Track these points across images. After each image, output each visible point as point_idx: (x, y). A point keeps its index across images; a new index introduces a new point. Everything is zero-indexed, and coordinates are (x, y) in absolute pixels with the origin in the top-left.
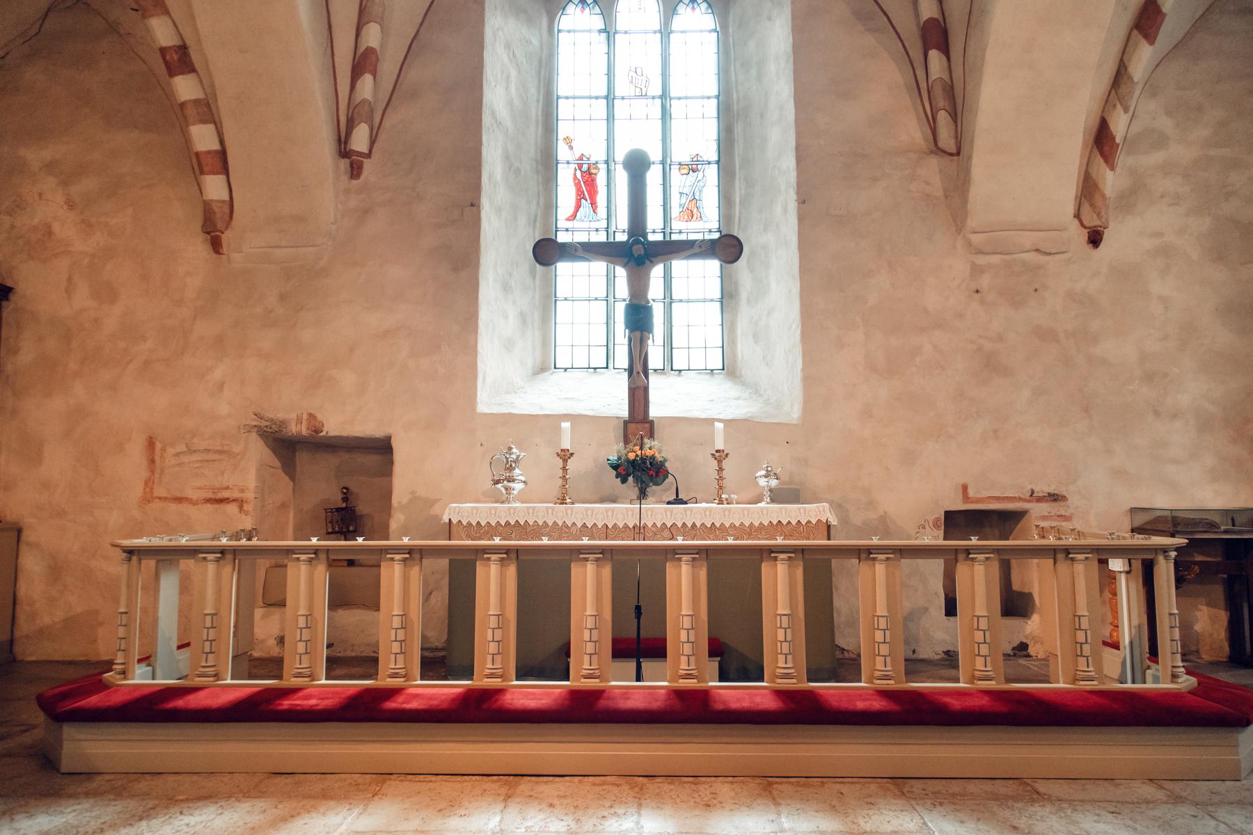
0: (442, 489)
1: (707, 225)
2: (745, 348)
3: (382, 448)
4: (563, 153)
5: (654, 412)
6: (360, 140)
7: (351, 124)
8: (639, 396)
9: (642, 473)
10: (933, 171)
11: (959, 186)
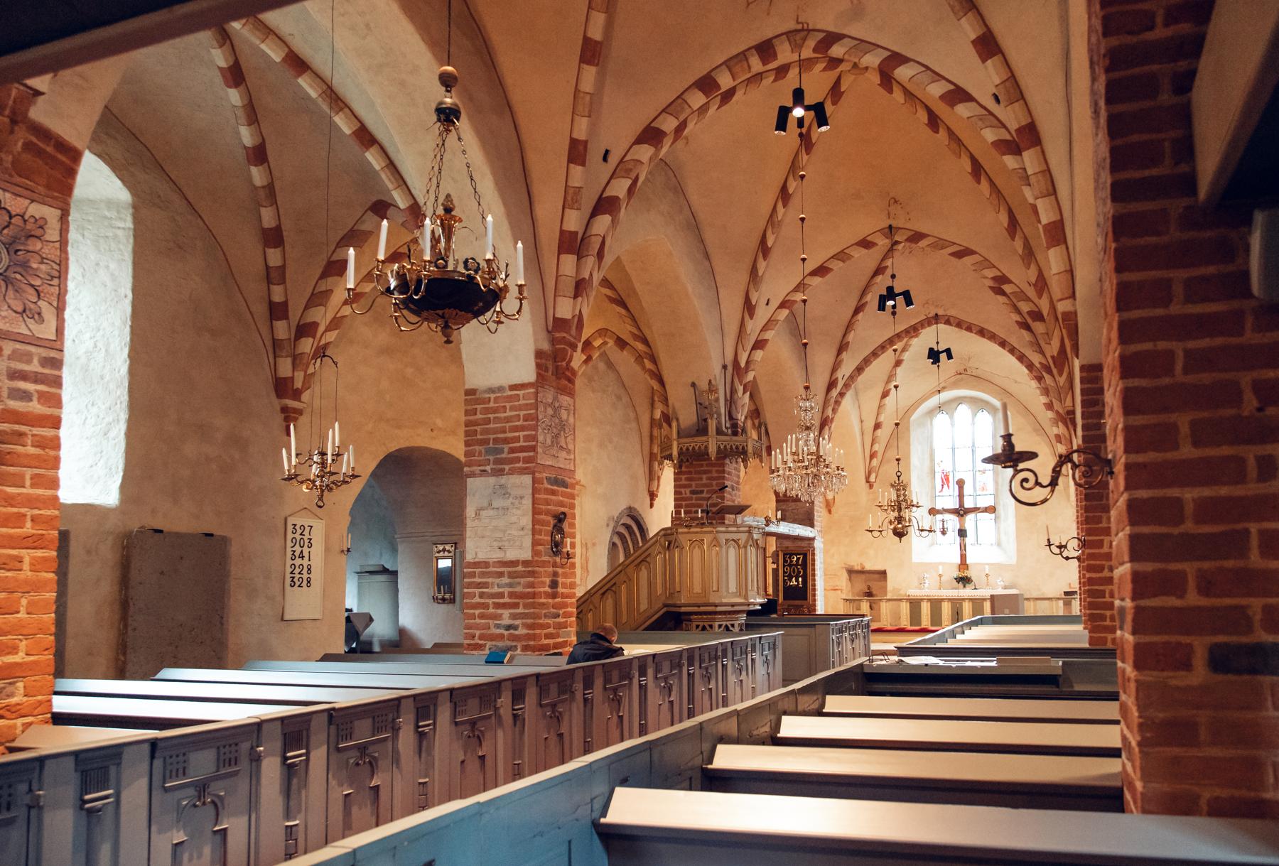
0: (901, 583)
1: (988, 502)
2: (1003, 538)
3: (884, 573)
5: (968, 562)
6: (872, 478)
8: (963, 557)
9: (964, 581)
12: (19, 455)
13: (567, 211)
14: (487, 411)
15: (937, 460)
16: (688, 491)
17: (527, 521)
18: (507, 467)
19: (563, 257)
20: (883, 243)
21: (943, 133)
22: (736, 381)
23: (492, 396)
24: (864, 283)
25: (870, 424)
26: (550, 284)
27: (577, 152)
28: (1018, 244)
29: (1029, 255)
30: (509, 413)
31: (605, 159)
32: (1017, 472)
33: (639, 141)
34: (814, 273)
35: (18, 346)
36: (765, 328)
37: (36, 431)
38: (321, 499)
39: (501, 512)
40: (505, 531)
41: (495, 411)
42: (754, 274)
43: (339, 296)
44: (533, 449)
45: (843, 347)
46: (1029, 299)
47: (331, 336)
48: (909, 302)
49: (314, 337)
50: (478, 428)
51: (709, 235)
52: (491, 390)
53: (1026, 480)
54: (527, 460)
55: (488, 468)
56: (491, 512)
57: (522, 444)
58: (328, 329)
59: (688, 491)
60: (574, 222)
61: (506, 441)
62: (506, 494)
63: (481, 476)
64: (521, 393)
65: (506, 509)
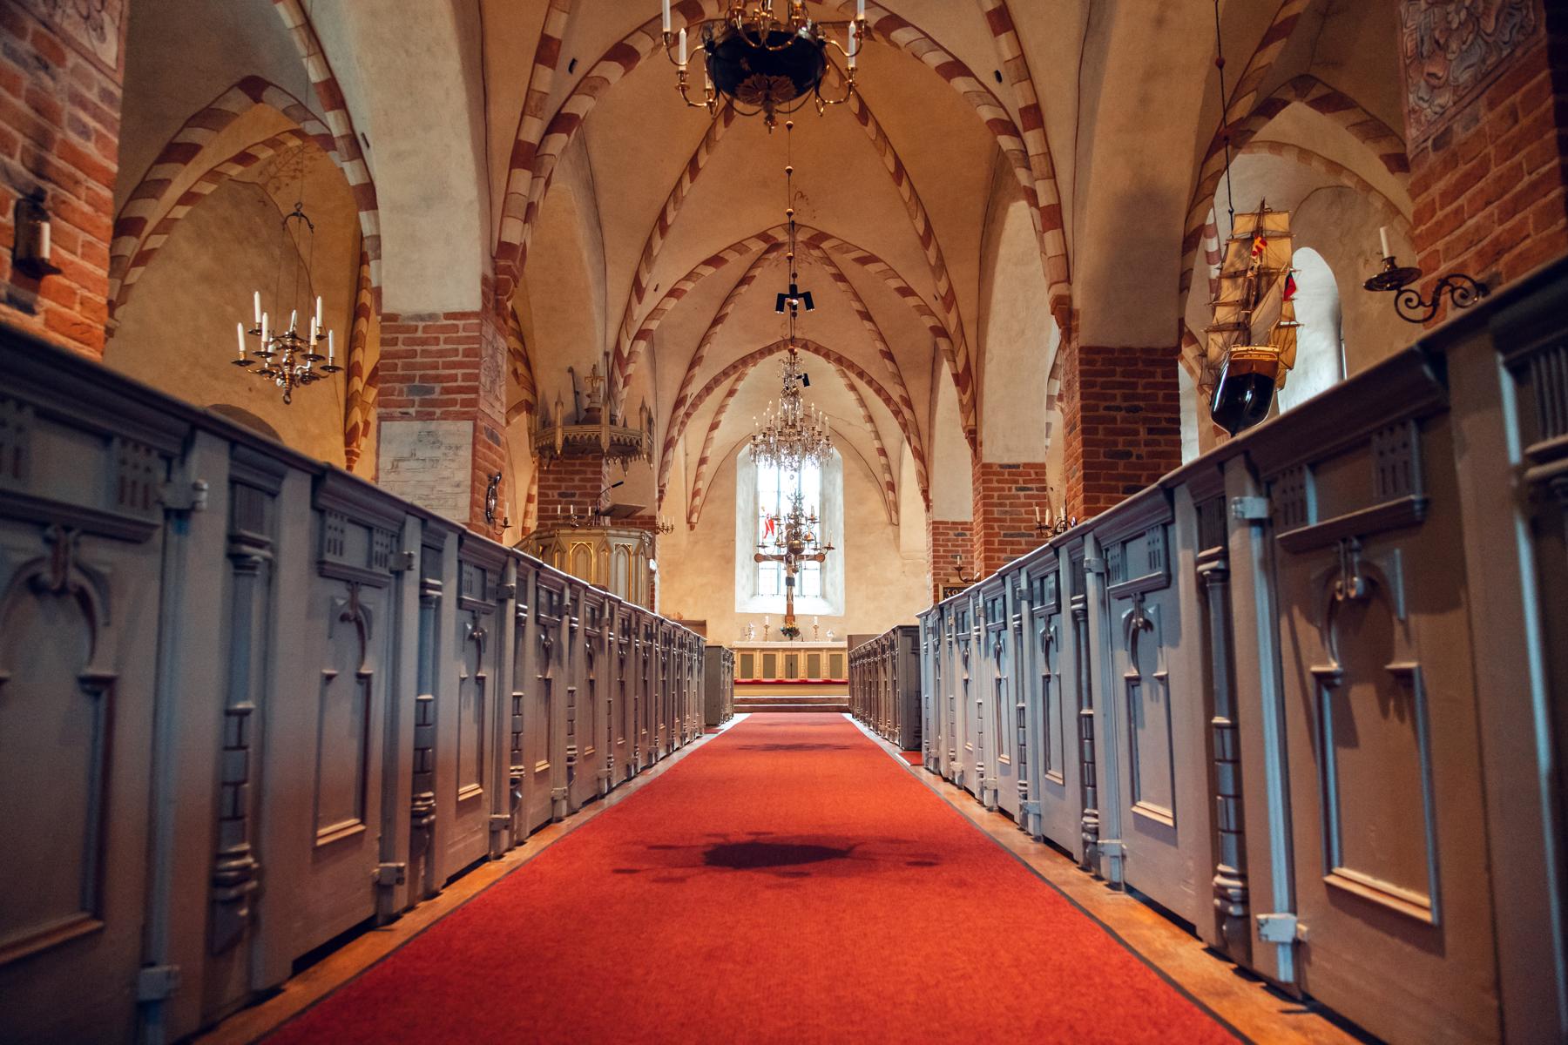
4: (761, 513)
6: (694, 519)
7: (691, 513)
8: (790, 607)
9: (791, 632)
10: (890, 529)
11: (897, 536)
12: (74, 210)
13: (527, 118)
14: (414, 341)
15: (761, 505)
16: (556, 493)
17: (464, 476)
18: (438, 411)
19: (517, 172)
20: (758, 247)
21: (870, 128)
22: (617, 372)
23: (421, 324)
24: (724, 294)
25: (695, 458)
26: (499, 200)
27: (547, 52)
28: (932, 253)
29: (940, 268)
30: (442, 346)
31: (571, 70)
32: (1400, 293)
33: (609, 56)
34: (708, 262)
35: (81, 61)
36: (650, 317)
37: (92, 184)
38: (288, 394)
39: (428, 464)
40: (432, 488)
41: (424, 342)
42: (647, 253)
43: (175, 191)
44: (475, 390)
45: (695, 362)
46: (932, 314)
47: (156, 242)
48: (809, 305)
49: (138, 236)
50: (399, 362)
51: (604, 200)
52: (420, 317)
53: (1409, 300)
54: (465, 403)
55: (412, 411)
56: (413, 464)
57: (460, 383)
58: (154, 232)
59: (556, 493)
60: (533, 131)
61: (437, 379)
62: (436, 443)
63: (402, 419)
64: (461, 323)
65: (435, 461)
